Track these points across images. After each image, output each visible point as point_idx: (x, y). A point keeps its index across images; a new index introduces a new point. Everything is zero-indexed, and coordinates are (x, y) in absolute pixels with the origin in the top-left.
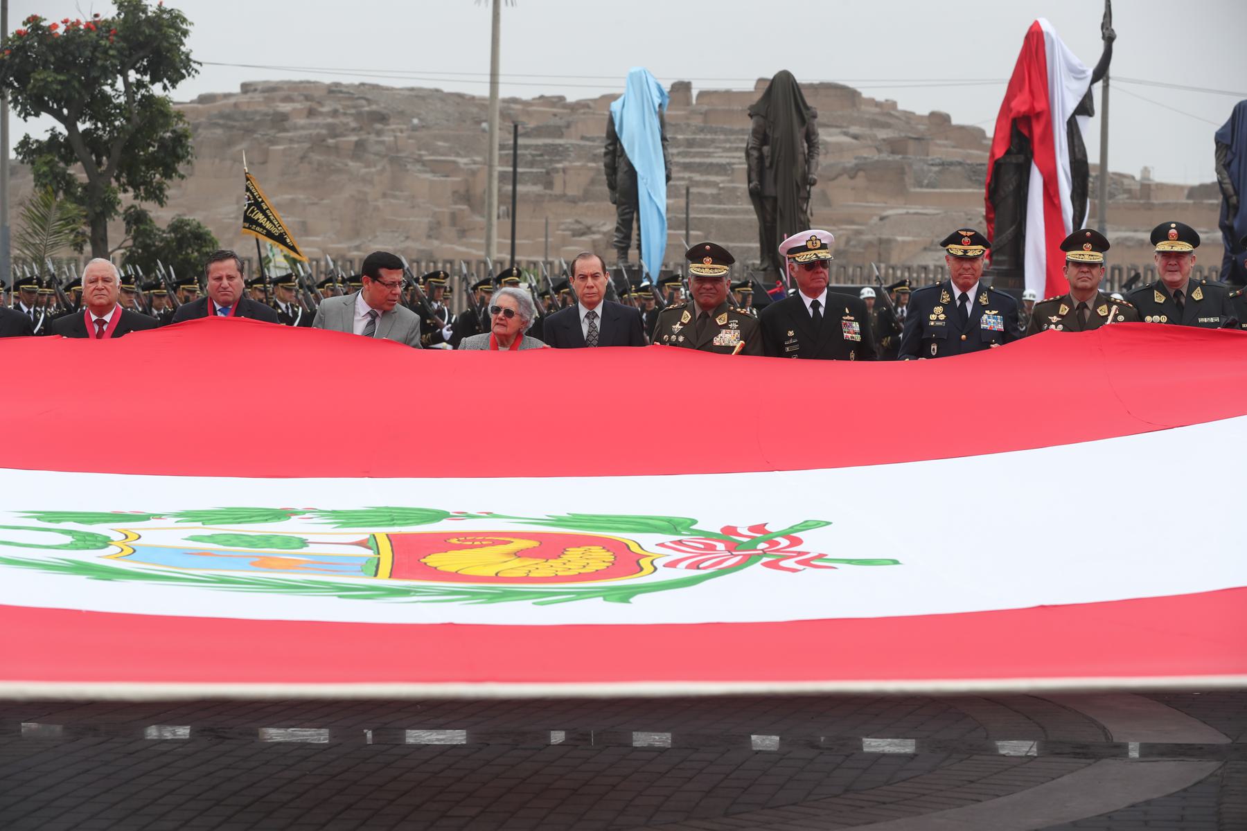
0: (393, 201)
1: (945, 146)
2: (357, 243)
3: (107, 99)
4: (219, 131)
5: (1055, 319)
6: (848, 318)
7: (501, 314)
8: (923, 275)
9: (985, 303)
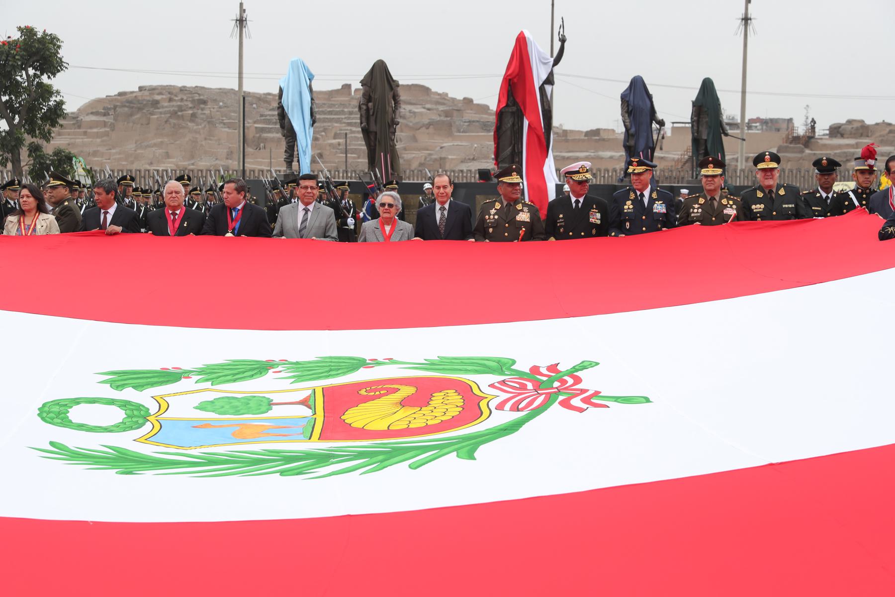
0: (210, 142)
1: (471, 113)
2: (192, 162)
3: (18, 84)
4: (126, 109)
5: (696, 206)
6: (594, 210)
7: (386, 207)
8: (461, 174)
9: (655, 197)
